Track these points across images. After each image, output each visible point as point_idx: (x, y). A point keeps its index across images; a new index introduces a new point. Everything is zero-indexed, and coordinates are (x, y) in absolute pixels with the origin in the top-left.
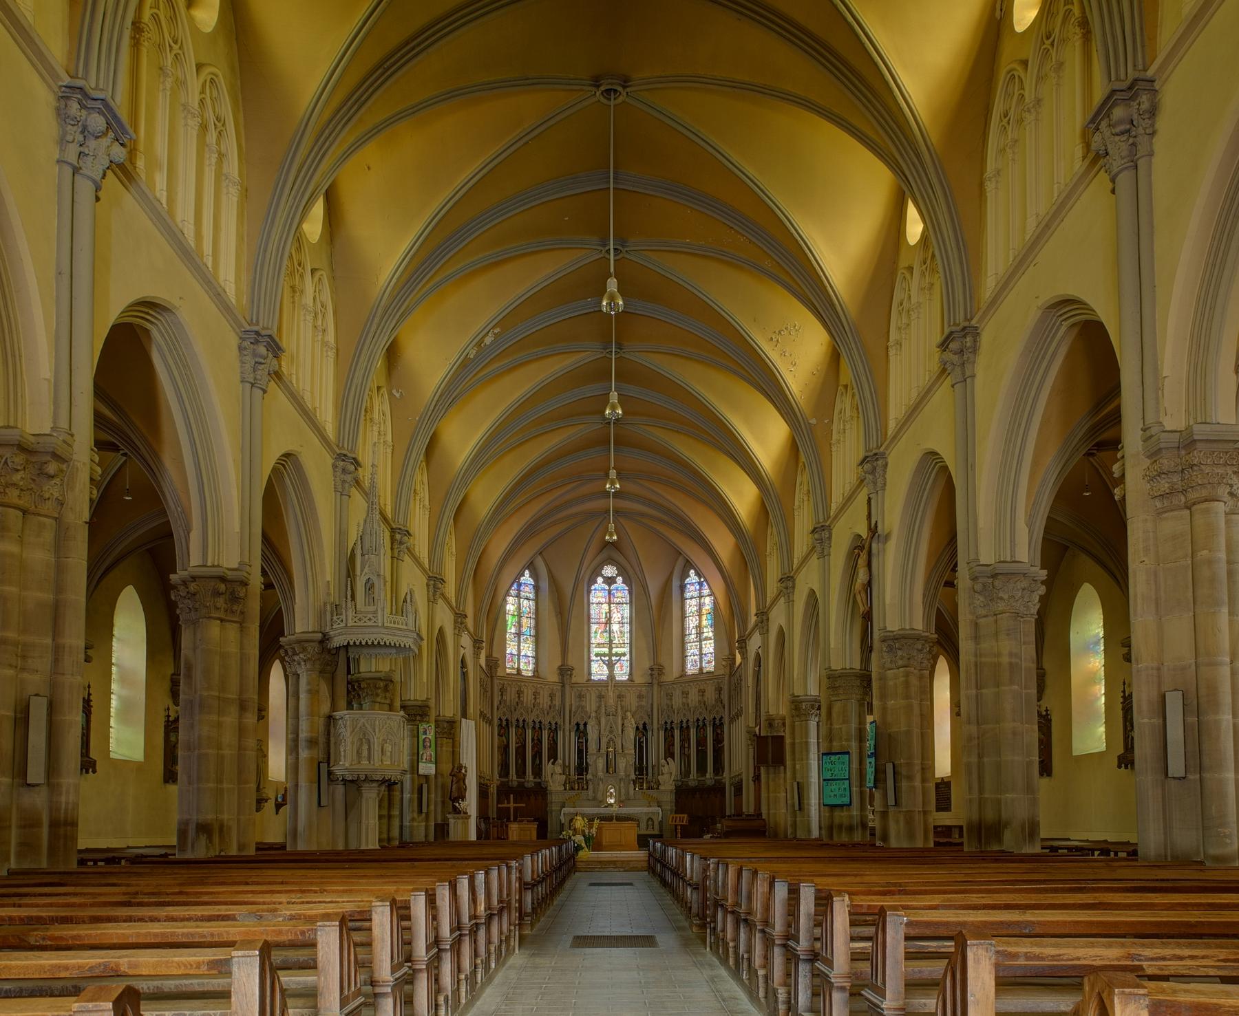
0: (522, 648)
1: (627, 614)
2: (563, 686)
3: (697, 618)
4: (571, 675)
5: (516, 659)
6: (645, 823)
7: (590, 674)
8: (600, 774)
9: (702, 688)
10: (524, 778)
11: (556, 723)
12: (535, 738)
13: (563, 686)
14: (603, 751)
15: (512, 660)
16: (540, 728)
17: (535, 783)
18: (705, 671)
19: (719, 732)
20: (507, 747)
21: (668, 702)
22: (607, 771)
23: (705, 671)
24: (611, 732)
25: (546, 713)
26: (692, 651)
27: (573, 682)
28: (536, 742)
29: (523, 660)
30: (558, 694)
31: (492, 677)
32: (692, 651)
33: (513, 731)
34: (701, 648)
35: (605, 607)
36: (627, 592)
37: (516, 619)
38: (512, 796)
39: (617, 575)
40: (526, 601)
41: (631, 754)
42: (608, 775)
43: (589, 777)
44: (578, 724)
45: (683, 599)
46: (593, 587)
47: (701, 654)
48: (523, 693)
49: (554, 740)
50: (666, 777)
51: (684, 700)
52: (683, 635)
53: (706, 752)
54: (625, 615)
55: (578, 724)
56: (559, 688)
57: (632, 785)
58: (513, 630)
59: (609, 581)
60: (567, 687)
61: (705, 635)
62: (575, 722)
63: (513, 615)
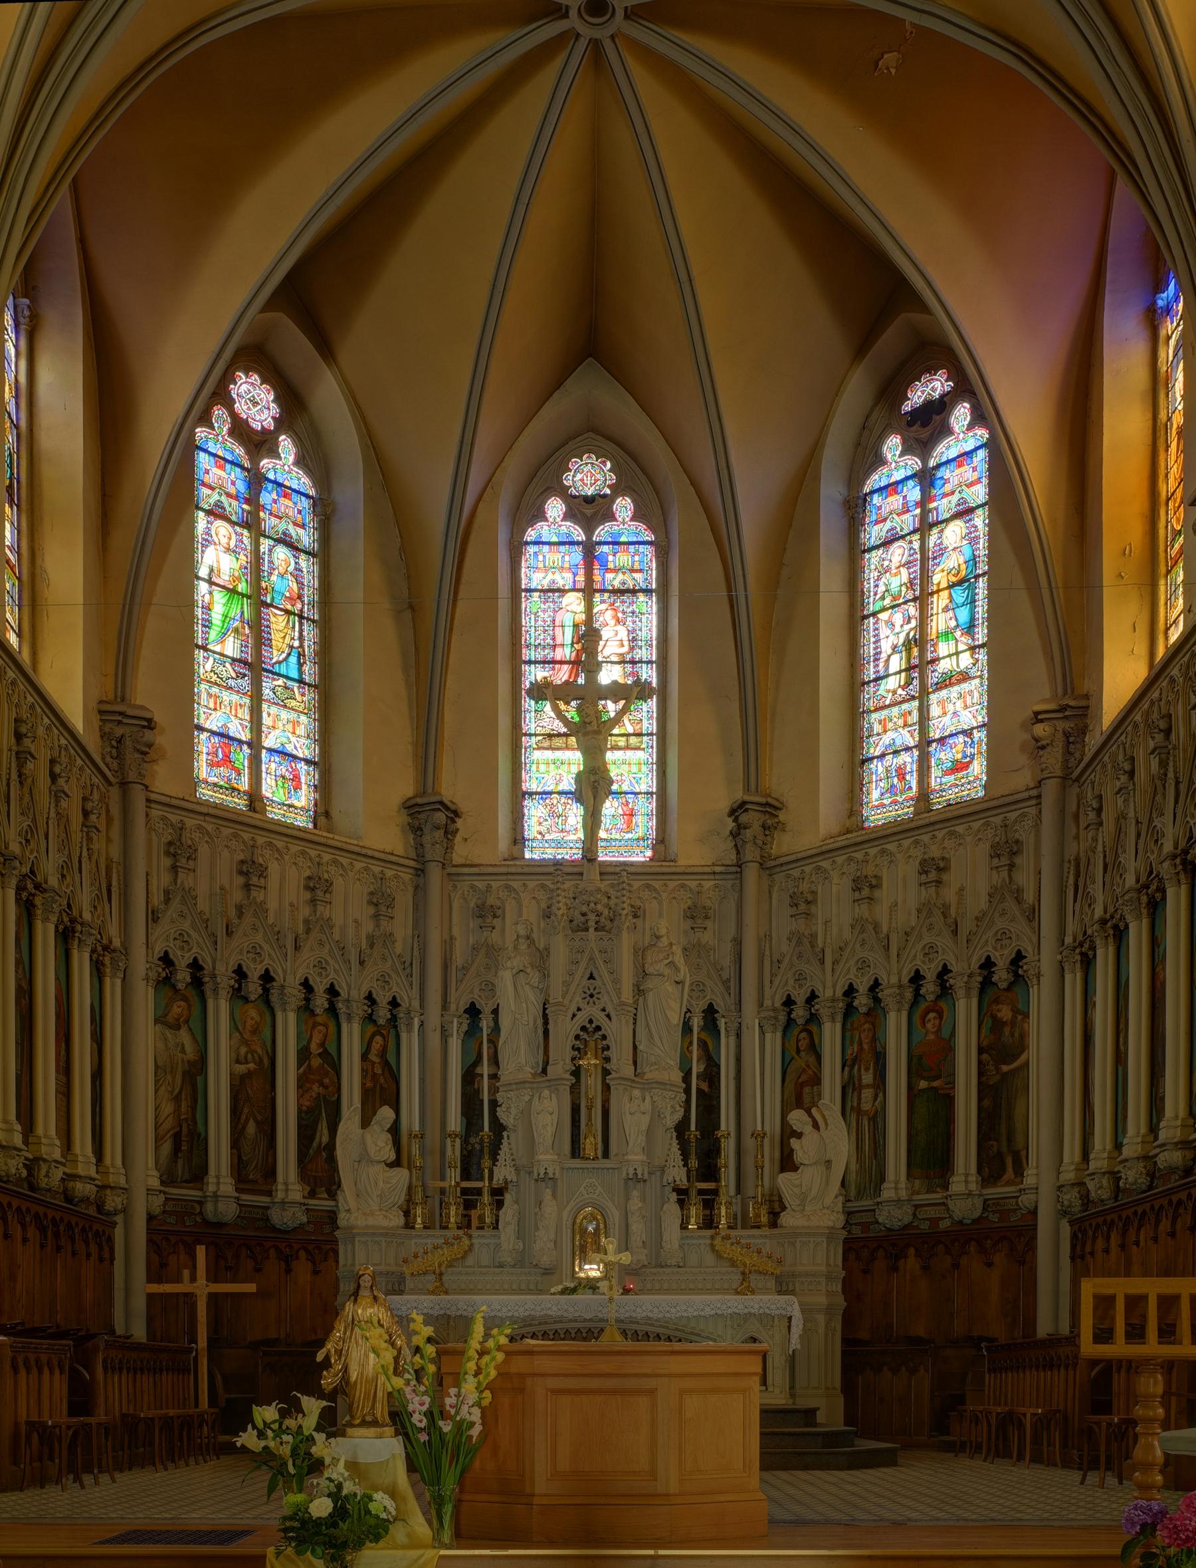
0: (267, 720)
1: (649, 626)
2: (420, 872)
3: (912, 610)
4: (449, 833)
5: (242, 757)
7: (518, 840)
8: (548, 1159)
9: (935, 852)
10: (269, 1193)
11: (394, 1003)
13: (420, 872)
14: (560, 1067)
15: (227, 760)
16: (332, 1010)
18: (938, 802)
19: (1005, 1013)
20: (196, 1070)
22: (576, 1150)
23: (938, 802)
26: (886, 739)
27: (457, 860)
29: (271, 767)
30: (404, 900)
31: (124, 785)
32: (886, 739)
33: (220, 1010)
34: (924, 717)
35: (574, 604)
36: (648, 551)
37: (241, 609)
38: (201, 1251)
40: (281, 553)
42: (577, 1163)
43: (503, 1172)
45: (855, 553)
46: (531, 534)
47: (925, 743)
48: (263, 873)
49: (386, 1064)
51: (863, 910)
52: (855, 684)
53: (949, 1100)
54: (643, 635)
56: (406, 876)
57: (672, 1209)
58: (231, 647)
59: (589, 510)
60: (435, 875)
61: (944, 666)
62: (464, 1004)
63: (233, 591)
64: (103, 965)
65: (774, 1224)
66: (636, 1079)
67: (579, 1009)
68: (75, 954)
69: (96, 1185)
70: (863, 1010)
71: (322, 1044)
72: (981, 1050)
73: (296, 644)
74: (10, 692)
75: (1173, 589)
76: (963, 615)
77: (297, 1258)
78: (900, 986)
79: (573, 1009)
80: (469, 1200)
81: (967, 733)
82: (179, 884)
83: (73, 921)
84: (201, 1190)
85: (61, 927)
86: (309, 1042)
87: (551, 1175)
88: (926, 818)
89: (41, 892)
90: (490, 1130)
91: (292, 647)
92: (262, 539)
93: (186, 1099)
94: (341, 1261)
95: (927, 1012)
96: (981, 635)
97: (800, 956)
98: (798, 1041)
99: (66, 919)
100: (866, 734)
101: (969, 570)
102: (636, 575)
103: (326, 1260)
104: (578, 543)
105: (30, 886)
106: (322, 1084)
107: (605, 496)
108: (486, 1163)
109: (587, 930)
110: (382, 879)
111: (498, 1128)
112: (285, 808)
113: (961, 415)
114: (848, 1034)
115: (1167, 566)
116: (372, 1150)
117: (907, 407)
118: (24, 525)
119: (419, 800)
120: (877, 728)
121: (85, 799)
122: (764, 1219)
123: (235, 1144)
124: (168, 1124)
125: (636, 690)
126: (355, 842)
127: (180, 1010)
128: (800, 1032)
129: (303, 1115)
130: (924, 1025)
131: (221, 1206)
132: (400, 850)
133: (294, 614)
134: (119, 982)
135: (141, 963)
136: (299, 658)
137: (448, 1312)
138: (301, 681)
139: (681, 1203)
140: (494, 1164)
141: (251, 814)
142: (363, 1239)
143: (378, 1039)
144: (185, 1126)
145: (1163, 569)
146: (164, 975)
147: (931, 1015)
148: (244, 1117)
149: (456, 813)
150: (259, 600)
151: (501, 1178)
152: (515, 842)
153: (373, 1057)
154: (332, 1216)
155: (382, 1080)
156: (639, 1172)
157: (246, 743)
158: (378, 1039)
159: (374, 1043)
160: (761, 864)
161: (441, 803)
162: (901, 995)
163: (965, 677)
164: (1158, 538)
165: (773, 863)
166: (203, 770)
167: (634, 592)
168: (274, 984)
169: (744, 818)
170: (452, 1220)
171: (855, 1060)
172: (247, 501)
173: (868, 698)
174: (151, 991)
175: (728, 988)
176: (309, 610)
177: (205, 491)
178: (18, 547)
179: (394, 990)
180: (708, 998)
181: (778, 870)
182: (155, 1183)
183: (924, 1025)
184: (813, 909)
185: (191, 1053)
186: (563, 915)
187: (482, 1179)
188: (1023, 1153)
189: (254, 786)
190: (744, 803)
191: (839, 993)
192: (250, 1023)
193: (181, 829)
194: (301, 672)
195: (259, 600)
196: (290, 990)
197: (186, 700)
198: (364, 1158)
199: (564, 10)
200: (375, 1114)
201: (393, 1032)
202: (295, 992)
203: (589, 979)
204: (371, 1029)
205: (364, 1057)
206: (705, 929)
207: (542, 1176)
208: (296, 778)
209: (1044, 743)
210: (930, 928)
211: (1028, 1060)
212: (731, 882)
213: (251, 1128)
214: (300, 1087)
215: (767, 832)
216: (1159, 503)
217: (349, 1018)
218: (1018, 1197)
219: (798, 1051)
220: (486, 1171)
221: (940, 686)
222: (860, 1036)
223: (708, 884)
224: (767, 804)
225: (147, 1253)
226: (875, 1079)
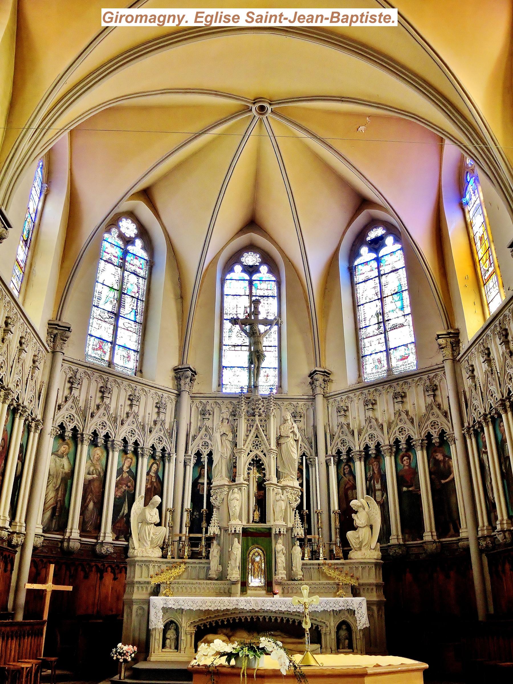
2: (179, 395)
5: (107, 347)
6: (333, 636)
7: (220, 384)
11: (163, 450)
12: (125, 469)
13: (179, 395)
15: (101, 348)
16: (135, 452)
17: (115, 547)
19: (440, 457)
21: (342, 420)
23: (396, 373)
24: (256, 446)
25: (147, 429)
28: (125, 475)
29: (119, 352)
30: (170, 407)
31: (54, 353)
33: (85, 449)
39: (261, 263)
41: (293, 488)
43: (213, 530)
44: (198, 454)
46: (228, 277)
47: (388, 350)
50: (363, 533)
51: (370, 414)
53: (419, 497)
55: (198, 454)
56: (173, 397)
59: (251, 270)
60: (186, 398)
64: (31, 427)
65: (346, 556)
66: (278, 484)
67: (251, 451)
68: (17, 420)
69: (8, 532)
70: (373, 456)
71: (129, 467)
72: (431, 473)
73: (135, 308)
74: (6, 306)
75: (488, 290)
76: (399, 304)
77: (107, 572)
78: (390, 445)
79: (248, 451)
80: (194, 542)
81: (406, 345)
82: (72, 394)
83: (18, 405)
84: (63, 535)
85: (12, 407)
86: (123, 466)
87: (237, 532)
88: (391, 378)
89: (4, 390)
90: (206, 508)
91: (133, 309)
92: (125, 271)
93: (61, 490)
94: (128, 575)
95: (403, 457)
96: (408, 310)
97: (343, 433)
98: (344, 469)
99: (15, 404)
100: (363, 347)
101: (399, 289)
102: (268, 291)
103: (121, 572)
104: (246, 280)
105: (30, 419)
106: (127, 485)
107: (257, 265)
108: (204, 525)
109: (255, 416)
110: (162, 397)
111: (210, 507)
112: (123, 368)
113: (389, 240)
114: (367, 466)
115: (484, 282)
116: (148, 517)
117: (368, 239)
118: (30, 254)
119: (180, 367)
120: (367, 344)
121: (35, 356)
122: (341, 555)
123: (82, 513)
124: (52, 502)
125: (275, 322)
126: (152, 382)
127: (65, 449)
128: (344, 466)
129: (117, 500)
130: (402, 463)
131: (71, 544)
132: (171, 387)
133: (135, 298)
134: (37, 435)
135: (50, 427)
136: (135, 313)
137: (183, 607)
138: (135, 321)
139: (301, 546)
140: (208, 525)
141: (108, 368)
142: (140, 564)
143: (155, 465)
144: (59, 503)
145: (482, 284)
146: (59, 433)
147: (405, 458)
148: (88, 500)
149: (195, 372)
150: (121, 292)
151: (212, 533)
152: (219, 385)
153: (152, 474)
154: (126, 549)
155: (155, 484)
156: (282, 531)
157: (110, 342)
158: (155, 465)
159: (153, 467)
160: (324, 395)
161: (189, 368)
162: (391, 449)
163: (402, 325)
164: (478, 273)
165: (328, 395)
166: (90, 351)
167: (268, 297)
168: (110, 439)
169: (316, 377)
170: (186, 554)
171: (372, 478)
172: (121, 259)
173: (363, 333)
174: (52, 440)
175: (311, 447)
176: (141, 297)
177: (105, 254)
178: (26, 262)
179: (164, 444)
180: (303, 450)
181: (330, 398)
182: (40, 531)
183: (402, 463)
184: (347, 413)
185: (67, 468)
186: (244, 409)
187: (201, 532)
188: (457, 521)
189: (111, 359)
190: (316, 371)
191: (362, 449)
192: (96, 456)
193: (77, 372)
194: (136, 318)
195: (121, 292)
196: (116, 442)
197: (86, 324)
198: (144, 521)
199: (250, 109)
200: (151, 499)
201: (162, 463)
202: (119, 443)
203: (256, 437)
204: (152, 461)
205: (148, 474)
206: (300, 421)
207: (277, 532)
208: (129, 357)
209: (443, 346)
210: (401, 420)
211: (454, 477)
212: (311, 402)
213: (91, 505)
214: (117, 486)
215: (325, 383)
216: (476, 262)
217: (143, 455)
218: (458, 543)
219: (344, 474)
220: (204, 529)
221: (392, 329)
222: (373, 467)
223: (301, 403)
224: (325, 372)
225: (30, 567)
226: (381, 486)
